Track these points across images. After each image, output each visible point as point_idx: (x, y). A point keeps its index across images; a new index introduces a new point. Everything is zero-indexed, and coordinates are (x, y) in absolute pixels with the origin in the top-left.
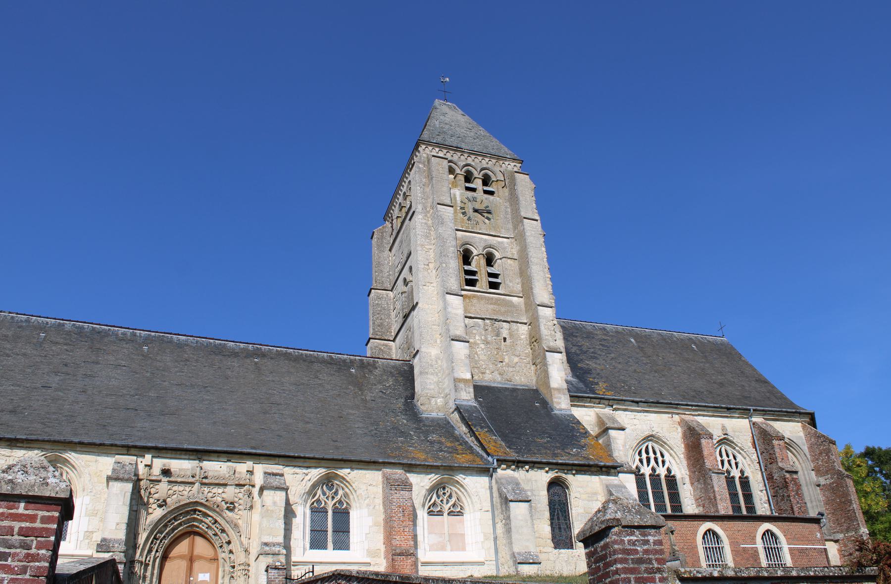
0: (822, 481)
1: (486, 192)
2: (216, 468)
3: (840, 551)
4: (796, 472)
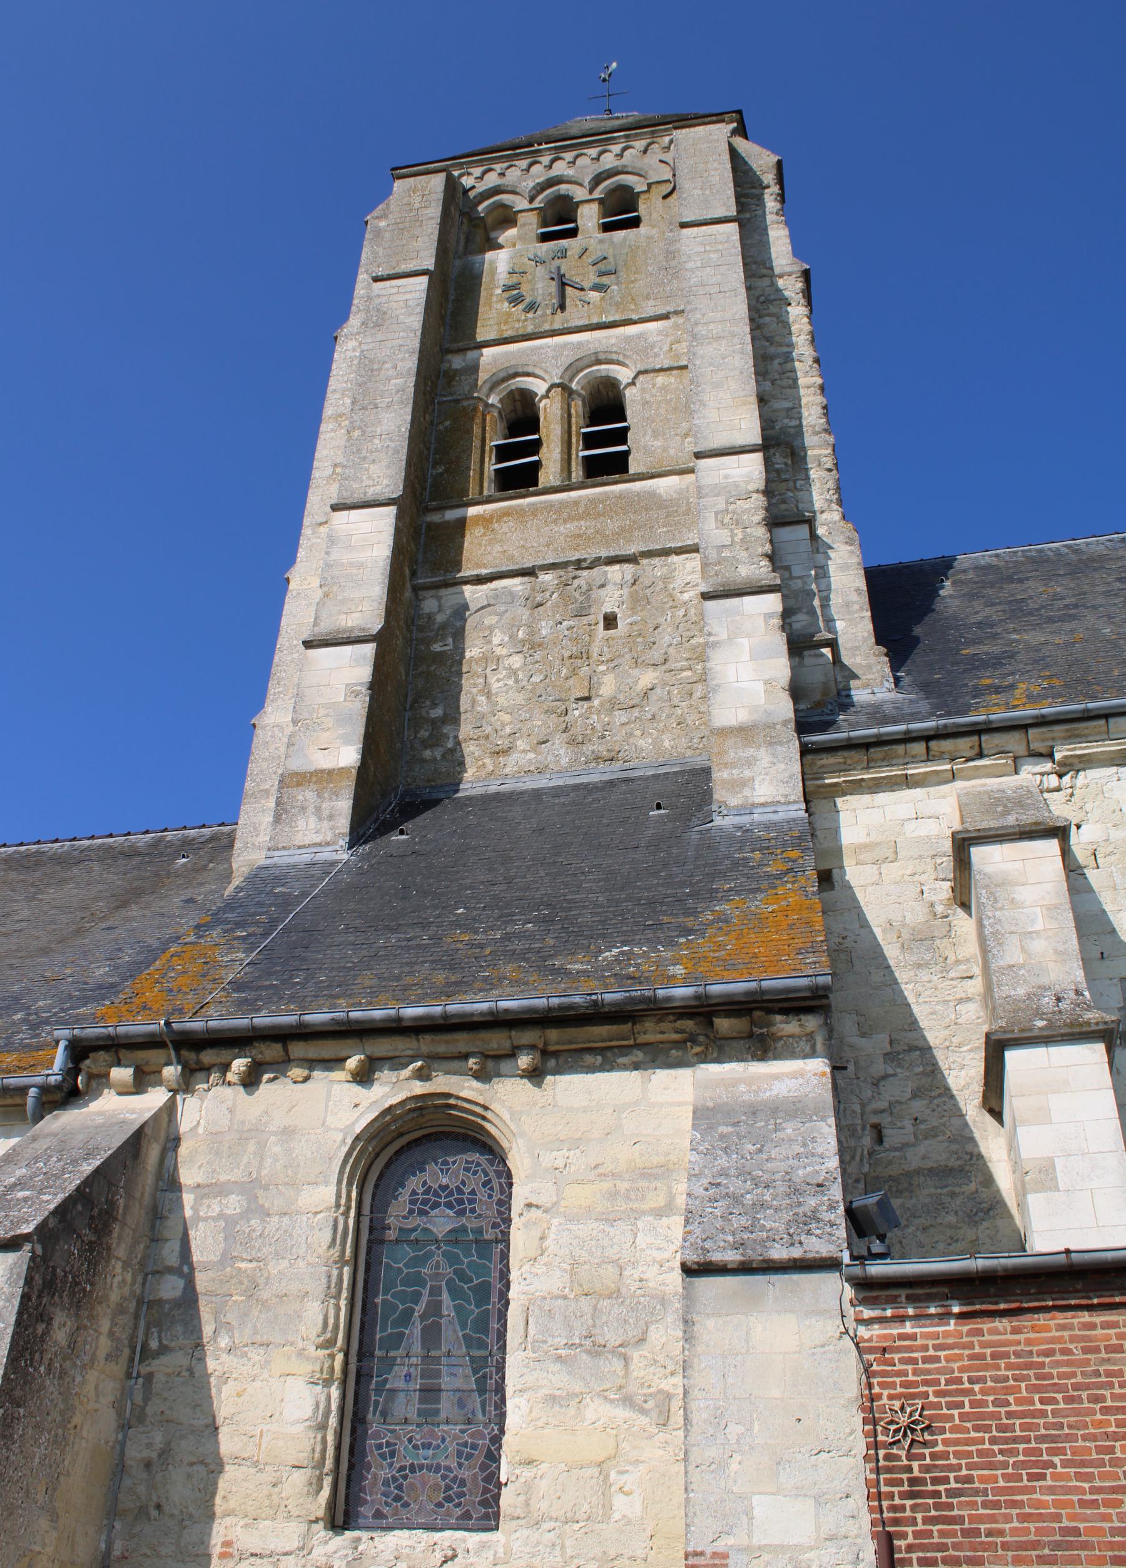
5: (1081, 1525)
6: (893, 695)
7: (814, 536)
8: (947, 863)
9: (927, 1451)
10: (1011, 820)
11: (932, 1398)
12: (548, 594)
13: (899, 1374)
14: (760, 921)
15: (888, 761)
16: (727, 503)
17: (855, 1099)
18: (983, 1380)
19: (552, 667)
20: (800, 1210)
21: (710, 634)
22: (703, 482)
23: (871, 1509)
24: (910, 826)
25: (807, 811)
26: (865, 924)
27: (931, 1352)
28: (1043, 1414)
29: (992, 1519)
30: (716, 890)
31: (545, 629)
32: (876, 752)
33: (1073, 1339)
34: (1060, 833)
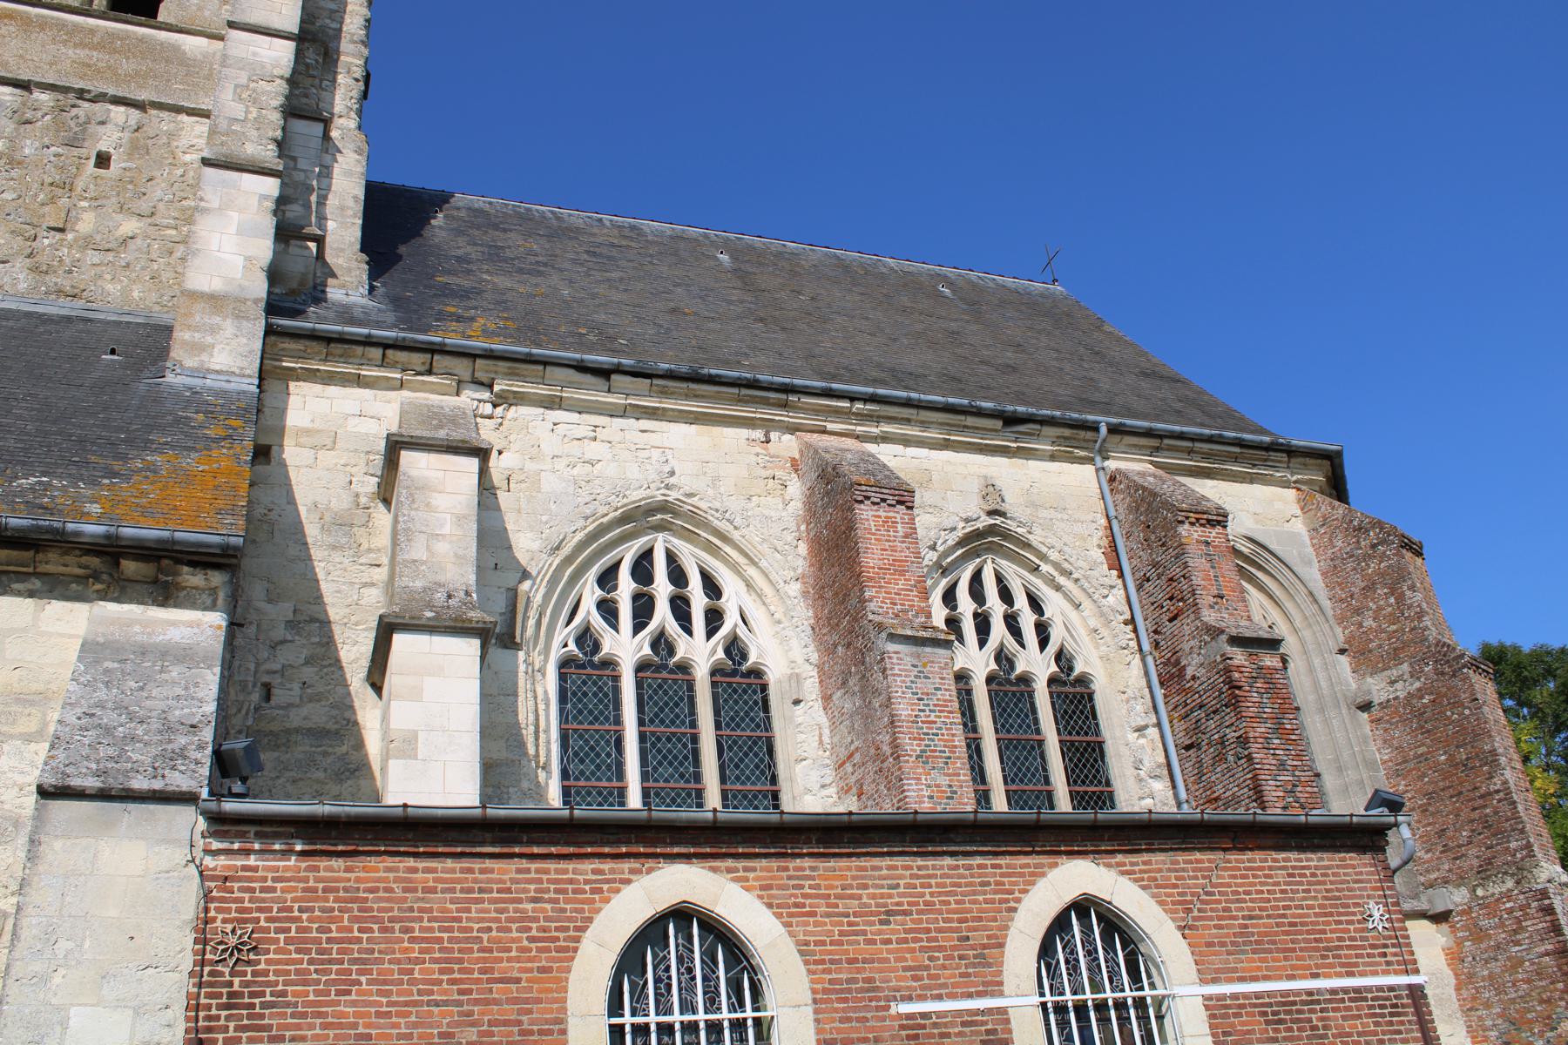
0: (1378, 688)
3: (1455, 957)
4: (1273, 644)
5: (373, 1032)
6: (364, 301)
7: (326, 136)
8: (379, 460)
9: (249, 969)
10: (442, 434)
11: (262, 923)
12: (40, 114)
13: (236, 900)
14: (188, 478)
15: (346, 358)
16: (250, 80)
17: (251, 658)
18: (312, 910)
19: (28, 188)
20: (170, 747)
21: (201, 199)
22: (230, 52)
23: (188, 1019)
24: (352, 422)
25: (259, 386)
26: (291, 501)
27: (269, 883)
28: (359, 940)
29: (298, 1027)
30: (152, 442)
31: (29, 149)
32: (337, 348)
33: (396, 880)
34: (482, 454)
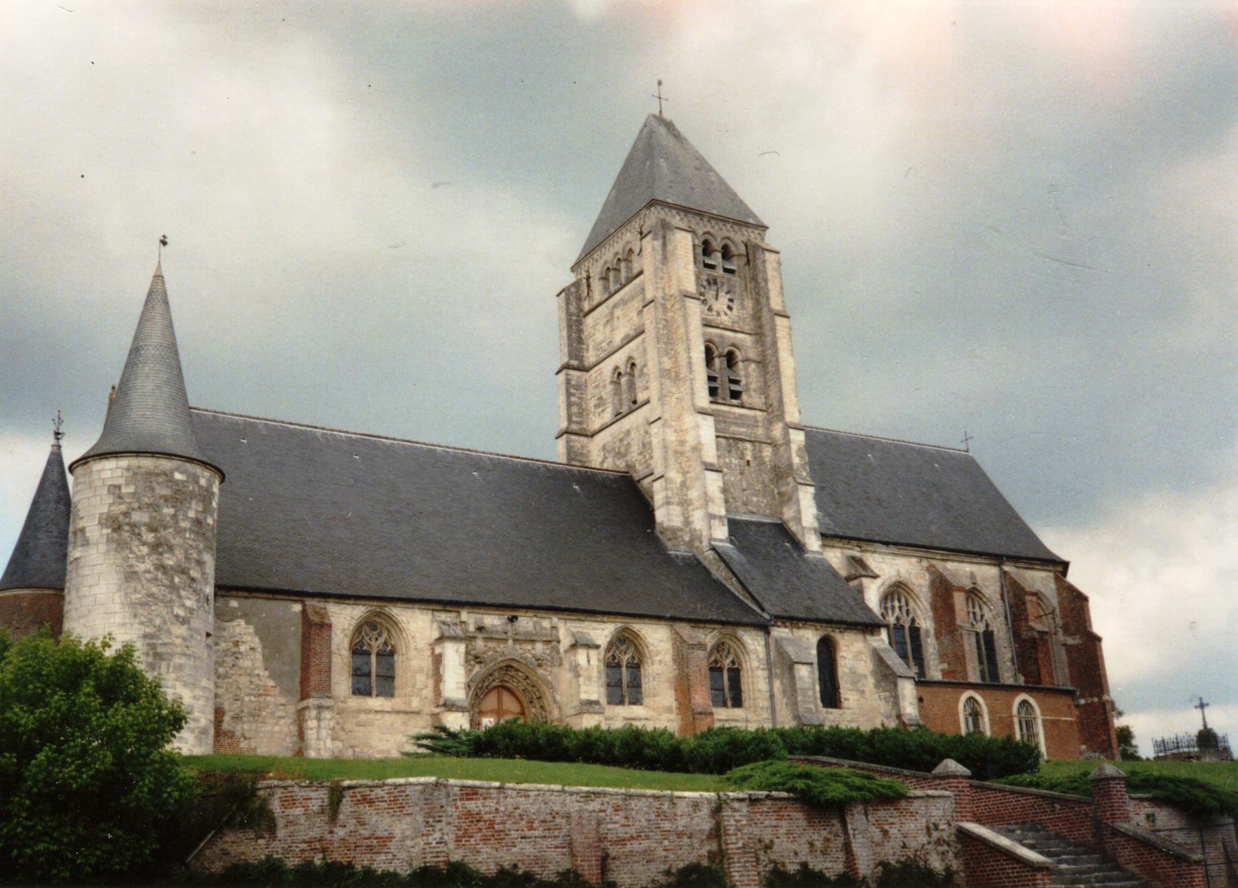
0: (1070, 641)
1: (726, 270)
2: (526, 622)
